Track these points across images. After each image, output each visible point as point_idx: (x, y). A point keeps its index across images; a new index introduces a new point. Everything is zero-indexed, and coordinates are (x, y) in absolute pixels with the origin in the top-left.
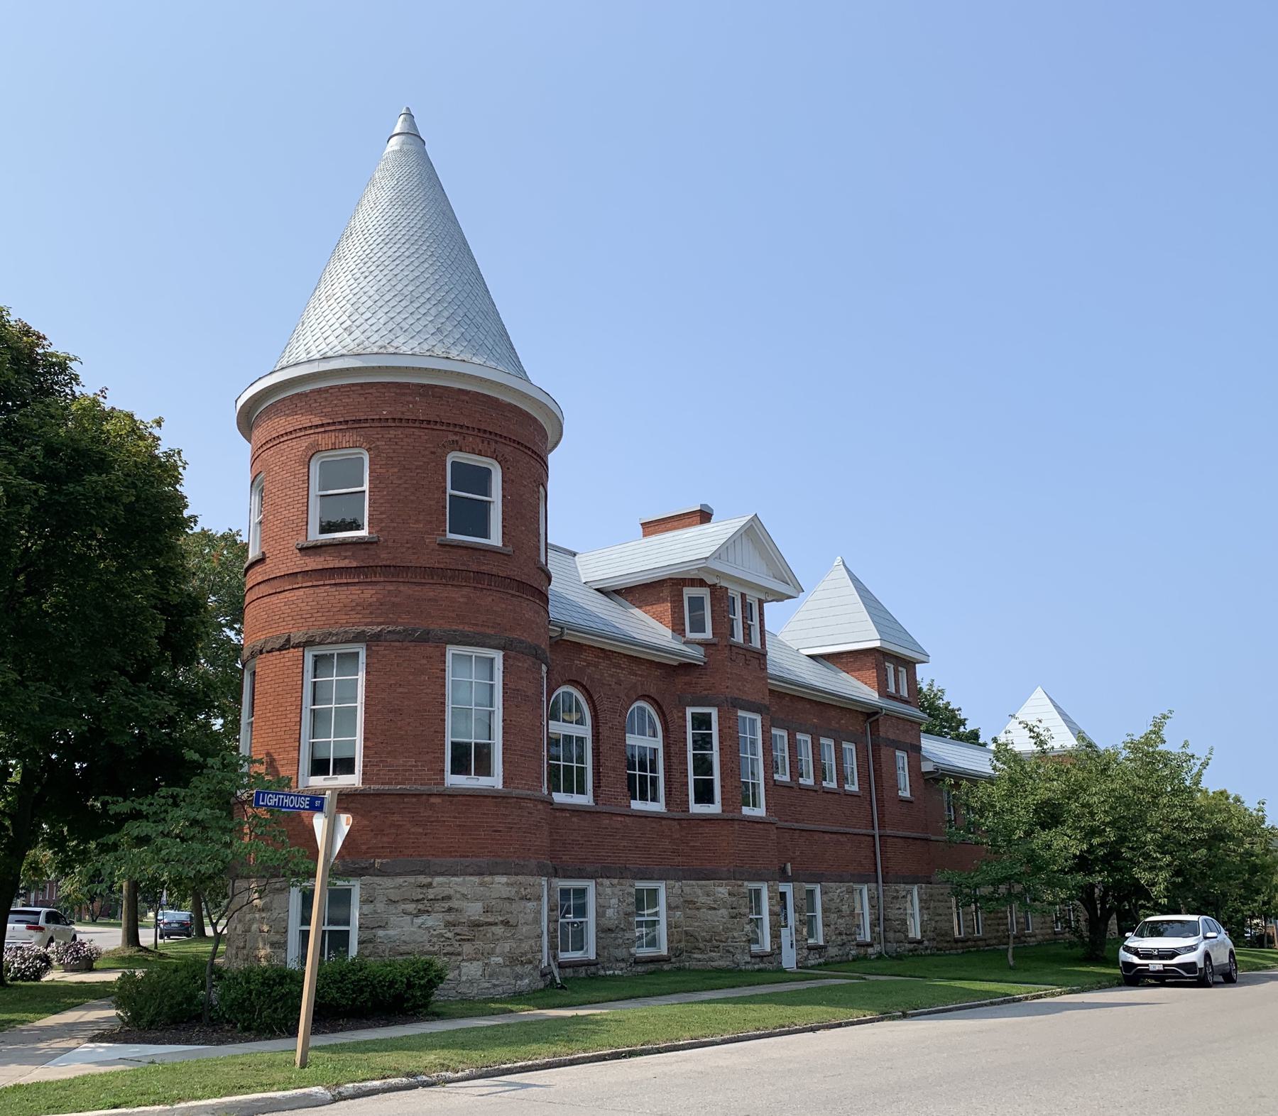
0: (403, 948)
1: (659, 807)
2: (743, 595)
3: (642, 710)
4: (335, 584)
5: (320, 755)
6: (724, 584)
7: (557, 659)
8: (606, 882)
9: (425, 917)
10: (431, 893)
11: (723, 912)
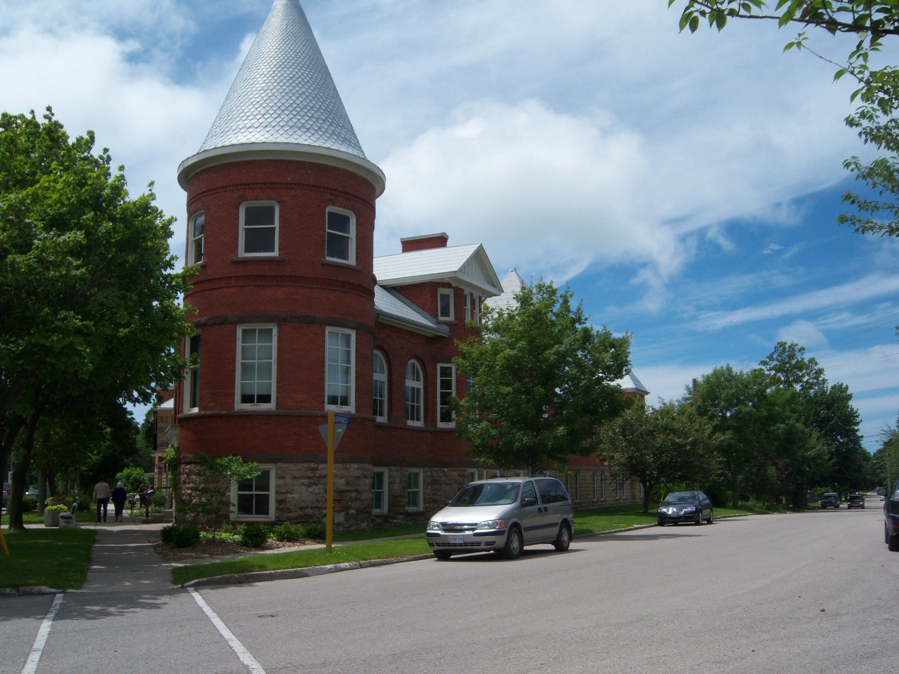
0: (302, 505)
1: (419, 424)
2: (471, 294)
3: (414, 364)
4: (258, 286)
5: (248, 392)
6: (462, 287)
7: (380, 334)
8: (394, 468)
9: (314, 487)
10: (318, 473)
11: (455, 486)
